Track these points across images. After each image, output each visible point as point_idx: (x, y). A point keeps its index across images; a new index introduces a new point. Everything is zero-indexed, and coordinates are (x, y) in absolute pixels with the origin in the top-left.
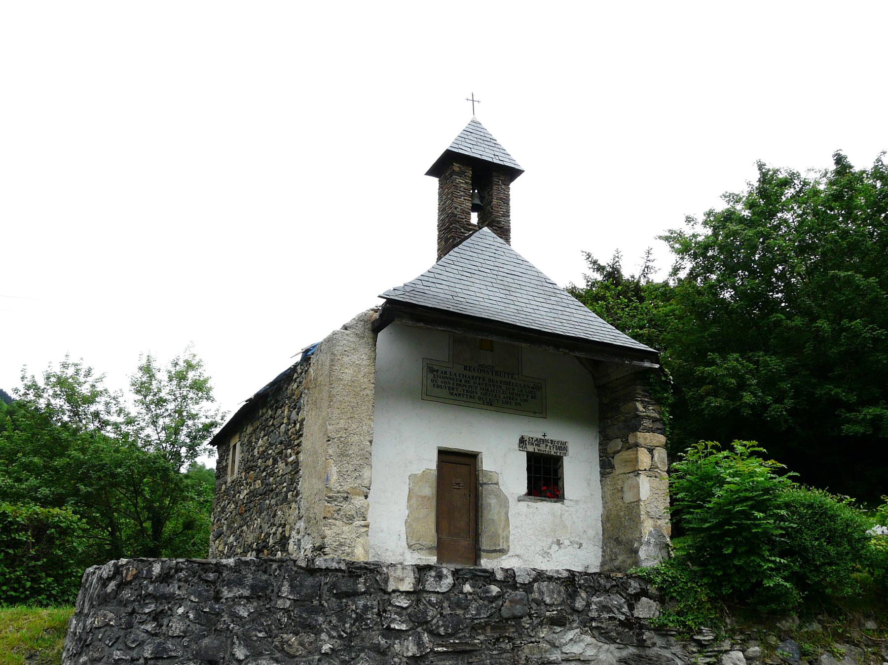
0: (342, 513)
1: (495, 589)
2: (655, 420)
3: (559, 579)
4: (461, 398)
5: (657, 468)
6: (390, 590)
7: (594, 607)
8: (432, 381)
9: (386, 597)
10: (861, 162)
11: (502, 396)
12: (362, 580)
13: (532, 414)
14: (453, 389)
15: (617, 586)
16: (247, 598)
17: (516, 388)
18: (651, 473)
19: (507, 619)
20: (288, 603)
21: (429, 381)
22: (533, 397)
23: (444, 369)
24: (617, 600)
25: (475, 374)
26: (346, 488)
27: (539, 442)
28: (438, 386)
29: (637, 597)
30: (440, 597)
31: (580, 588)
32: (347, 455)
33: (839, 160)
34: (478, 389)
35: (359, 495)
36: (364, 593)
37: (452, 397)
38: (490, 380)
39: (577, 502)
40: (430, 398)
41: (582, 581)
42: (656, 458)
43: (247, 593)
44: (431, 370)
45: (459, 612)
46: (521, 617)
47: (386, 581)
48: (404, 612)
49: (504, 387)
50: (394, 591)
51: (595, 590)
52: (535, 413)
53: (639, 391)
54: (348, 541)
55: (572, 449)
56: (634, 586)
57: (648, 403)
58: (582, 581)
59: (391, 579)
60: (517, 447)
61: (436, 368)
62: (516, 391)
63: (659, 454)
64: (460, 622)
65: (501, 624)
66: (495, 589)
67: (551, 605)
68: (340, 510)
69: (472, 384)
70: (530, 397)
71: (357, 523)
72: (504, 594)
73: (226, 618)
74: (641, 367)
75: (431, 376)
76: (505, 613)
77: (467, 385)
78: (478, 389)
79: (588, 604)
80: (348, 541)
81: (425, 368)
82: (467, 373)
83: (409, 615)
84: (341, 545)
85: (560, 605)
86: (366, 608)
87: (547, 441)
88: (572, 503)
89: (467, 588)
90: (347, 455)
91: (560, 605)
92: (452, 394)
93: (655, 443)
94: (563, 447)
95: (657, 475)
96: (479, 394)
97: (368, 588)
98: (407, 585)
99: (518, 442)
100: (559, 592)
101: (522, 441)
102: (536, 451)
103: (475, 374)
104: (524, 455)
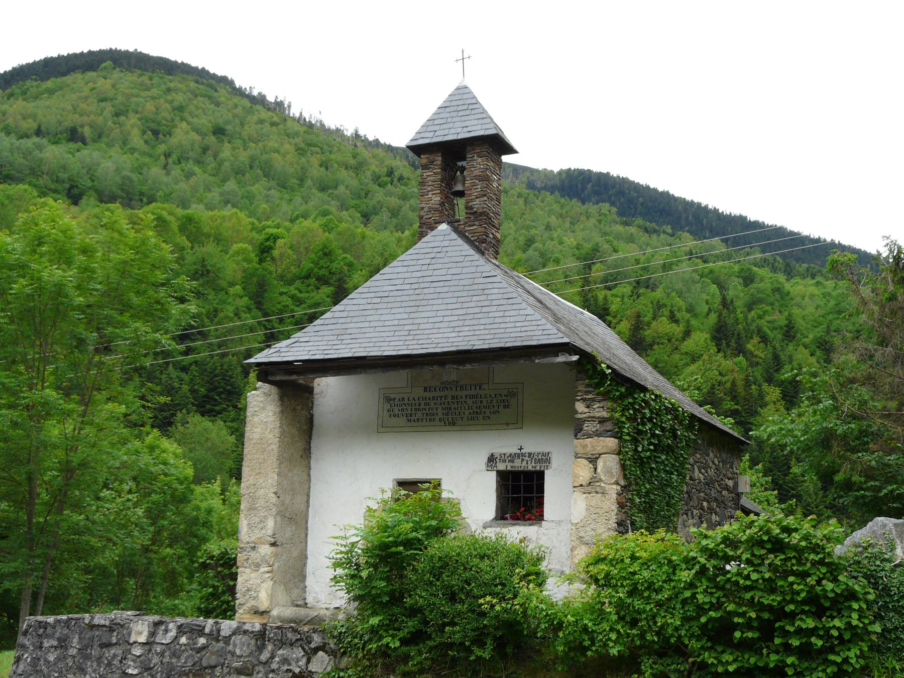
0: (250, 561)
1: (202, 641)
2: (602, 421)
3: (252, 632)
4: (420, 423)
5: (601, 480)
6: (131, 641)
7: (277, 659)
8: (389, 411)
9: (129, 647)
10: (361, 133)
11: (467, 412)
12: (115, 634)
13: (505, 427)
14: (411, 415)
15: (301, 639)
16: (56, 647)
17: (484, 401)
18: (590, 489)
19: (206, 668)
20: (75, 651)
21: (385, 412)
22: (505, 407)
23: (401, 396)
24: (298, 653)
25: (438, 394)
26: (253, 539)
27: (512, 457)
28: (395, 416)
29: (316, 650)
30: (164, 647)
31: (269, 641)
32: (255, 509)
33: (356, 131)
34: (440, 409)
35: (263, 543)
36: (116, 644)
37: (410, 424)
38: (453, 397)
39: (559, 522)
40: (387, 429)
41: (272, 635)
42: (599, 470)
43: (55, 643)
44: (388, 399)
45: (174, 660)
46: (215, 667)
47: (130, 634)
48: (138, 660)
49: (470, 401)
50: (135, 642)
51: (282, 643)
52: (507, 424)
53: (580, 388)
54: (254, 587)
55: (555, 462)
56: (317, 639)
57: (593, 400)
58: (272, 635)
59: (133, 633)
60: (484, 467)
61: (392, 396)
62: (485, 403)
63: (605, 463)
64: (172, 669)
65: (199, 672)
66: (202, 641)
67: (241, 657)
68: (248, 559)
69: (432, 405)
70: (501, 408)
71: (262, 570)
72: (208, 646)
73: (42, 662)
74: (553, 364)
75: (388, 406)
76: (204, 663)
77: (427, 407)
78: (440, 409)
79: (272, 657)
80: (254, 587)
81: (382, 399)
82: (427, 394)
83: (141, 662)
84: (249, 590)
85: (248, 656)
86: (115, 656)
87: (523, 455)
88: (554, 524)
89: (183, 640)
90: (255, 509)
91: (248, 656)
92: (410, 421)
93: (599, 449)
94: (546, 459)
95: (598, 489)
96: (440, 415)
97: (118, 640)
98: (142, 639)
99: (486, 460)
100: (249, 645)
101: (492, 459)
102: (509, 468)
103: (438, 394)
104: (493, 475)
